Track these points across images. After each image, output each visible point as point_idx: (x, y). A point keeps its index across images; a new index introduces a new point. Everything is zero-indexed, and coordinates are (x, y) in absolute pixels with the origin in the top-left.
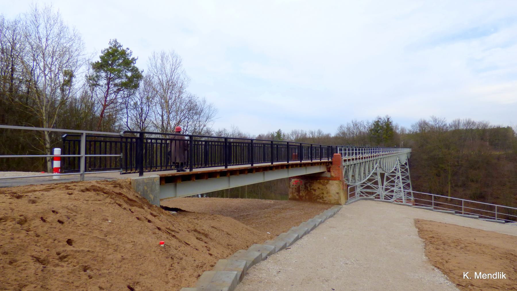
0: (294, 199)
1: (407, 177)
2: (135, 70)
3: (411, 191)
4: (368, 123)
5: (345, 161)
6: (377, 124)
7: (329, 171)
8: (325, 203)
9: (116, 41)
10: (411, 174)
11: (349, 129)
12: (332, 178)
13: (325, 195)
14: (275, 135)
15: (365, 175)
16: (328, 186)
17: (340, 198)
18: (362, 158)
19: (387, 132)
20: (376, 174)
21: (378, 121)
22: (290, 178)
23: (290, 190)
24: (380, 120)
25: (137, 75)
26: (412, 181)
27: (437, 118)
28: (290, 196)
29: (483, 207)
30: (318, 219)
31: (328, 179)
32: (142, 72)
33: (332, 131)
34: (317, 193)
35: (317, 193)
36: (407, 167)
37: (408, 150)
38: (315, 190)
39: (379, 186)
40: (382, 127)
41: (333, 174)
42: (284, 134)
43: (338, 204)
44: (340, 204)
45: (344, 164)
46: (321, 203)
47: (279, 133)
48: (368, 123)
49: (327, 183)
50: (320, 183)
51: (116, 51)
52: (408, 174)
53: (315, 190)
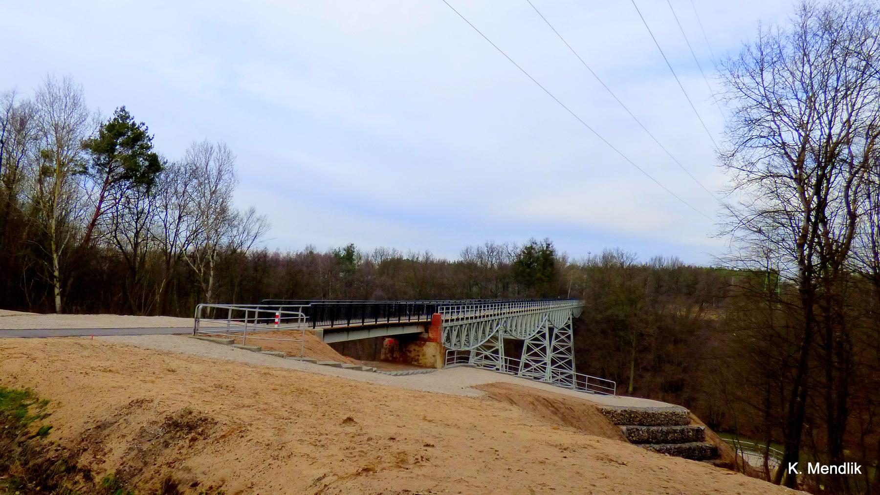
0: (386, 360)
1: (569, 350)
2: (154, 159)
3: (573, 372)
4: (515, 247)
5: (447, 321)
6: (529, 251)
7: (427, 331)
8: (420, 366)
9: (123, 110)
10: (575, 343)
11: (480, 256)
12: (430, 340)
13: (421, 357)
14: (343, 253)
15: (477, 340)
16: (424, 348)
17: (436, 361)
18: (480, 317)
19: (545, 268)
20: (495, 338)
21: (532, 248)
22: (384, 338)
23: (383, 351)
24: (534, 246)
25: (155, 164)
26: (576, 356)
27: (625, 252)
28: (382, 357)
29: (602, 383)
30: (411, 371)
31: (426, 340)
32: (165, 163)
33: (448, 250)
34: (413, 355)
35: (413, 355)
36: (571, 332)
37: (583, 303)
38: (410, 352)
39: (500, 356)
40: (538, 258)
41: (430, 335)
42: (358, 254)
43: (433, 367)
44: (434, 368)
45: (444, 325)
46: (416, 366)
47: (350, 252)
48: (515, 247)
49: (424, 345)
50: (416, 344)
51: (124, 125)
52: (571, 344)
53: (410, 352)
